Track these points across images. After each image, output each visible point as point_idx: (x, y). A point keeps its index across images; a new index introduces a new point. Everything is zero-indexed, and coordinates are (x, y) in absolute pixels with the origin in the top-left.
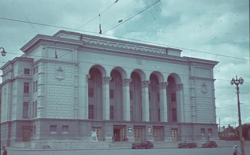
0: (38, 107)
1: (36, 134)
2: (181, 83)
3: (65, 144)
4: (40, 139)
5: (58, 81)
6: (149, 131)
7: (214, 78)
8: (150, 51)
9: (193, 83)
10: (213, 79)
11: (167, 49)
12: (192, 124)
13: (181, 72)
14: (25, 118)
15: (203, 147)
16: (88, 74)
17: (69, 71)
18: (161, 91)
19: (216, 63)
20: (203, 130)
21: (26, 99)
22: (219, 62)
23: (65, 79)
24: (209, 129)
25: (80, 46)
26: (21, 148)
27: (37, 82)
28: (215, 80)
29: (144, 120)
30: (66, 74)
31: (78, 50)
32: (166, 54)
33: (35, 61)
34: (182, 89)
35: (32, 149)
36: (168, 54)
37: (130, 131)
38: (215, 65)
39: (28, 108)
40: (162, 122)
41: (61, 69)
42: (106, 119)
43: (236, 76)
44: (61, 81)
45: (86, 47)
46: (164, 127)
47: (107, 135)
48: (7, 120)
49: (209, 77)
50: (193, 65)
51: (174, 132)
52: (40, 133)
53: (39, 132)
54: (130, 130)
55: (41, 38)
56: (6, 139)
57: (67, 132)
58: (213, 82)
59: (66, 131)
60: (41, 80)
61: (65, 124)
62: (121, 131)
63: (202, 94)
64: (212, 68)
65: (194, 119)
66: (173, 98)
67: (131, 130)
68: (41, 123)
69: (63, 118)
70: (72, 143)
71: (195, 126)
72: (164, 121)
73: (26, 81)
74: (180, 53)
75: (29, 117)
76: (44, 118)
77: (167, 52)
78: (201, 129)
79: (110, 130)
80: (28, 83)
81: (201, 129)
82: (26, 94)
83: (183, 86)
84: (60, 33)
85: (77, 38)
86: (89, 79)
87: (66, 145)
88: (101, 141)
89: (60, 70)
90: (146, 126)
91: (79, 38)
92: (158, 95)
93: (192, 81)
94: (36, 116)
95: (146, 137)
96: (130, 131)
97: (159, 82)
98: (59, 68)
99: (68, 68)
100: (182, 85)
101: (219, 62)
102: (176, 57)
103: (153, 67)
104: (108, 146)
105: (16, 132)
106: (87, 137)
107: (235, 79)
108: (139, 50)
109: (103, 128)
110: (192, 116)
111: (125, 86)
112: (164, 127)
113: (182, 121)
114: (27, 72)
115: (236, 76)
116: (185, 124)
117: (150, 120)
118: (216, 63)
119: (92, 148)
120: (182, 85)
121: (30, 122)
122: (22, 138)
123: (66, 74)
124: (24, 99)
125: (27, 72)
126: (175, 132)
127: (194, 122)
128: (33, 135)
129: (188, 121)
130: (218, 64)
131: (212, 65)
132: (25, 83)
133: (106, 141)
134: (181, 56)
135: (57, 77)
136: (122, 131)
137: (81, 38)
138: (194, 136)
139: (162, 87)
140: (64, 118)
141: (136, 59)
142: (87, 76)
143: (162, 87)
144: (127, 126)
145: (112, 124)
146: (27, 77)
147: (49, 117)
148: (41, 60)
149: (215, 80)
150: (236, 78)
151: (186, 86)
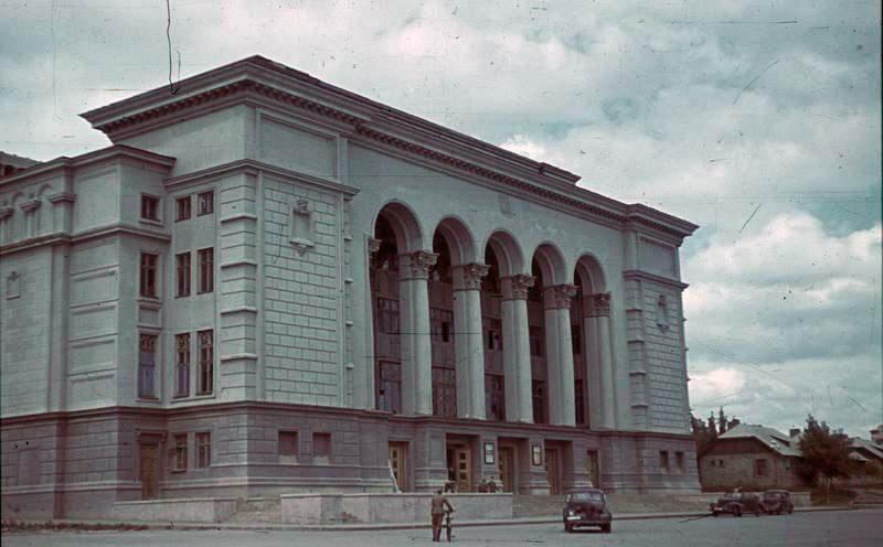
1: (213, 465)
2: (605, 292)
3: (401, 503)
4: (250, 486)
5: (297, 256)
6: (490, 459)
7: (683, 281)
9: (636, 293)
10: (679, 282)
12: (638, 437)
14: (146, 397)
15: (716, 514)
16: (373, 235)
20: (288, 436)
21: (150, 322)
22: (82, 115)
23: (318, 251)
24: (316, 435)
28: (686, 286)
29: (459, 416)
30: (320, 228)
33: (180, 171)
34: (608, 313)
35: (361, 522)
39: (153, 356)
40: (463, 417)
41: (305, 208)
42: (422, 412)
44: (306, 255)
45: (376, 136)
46: (569, 442)
47: (432, 471)
48: (43, 397)
49: (669, 276)
50: (636, 232)
52: (249, 459)
53: (246, 455)
55: (251, 78)
56: (51, 487)
57: (326, 458)
59: (322, 456)
60: (245, 245)
61: (322, 426)
62: (458, 456)
63: (657, 332)
68: (252, 422)
69: (327, 404)
70: (422, 500)
71: (647, 442)
73: (151, 248)
75: (158, 396)
76: (259, 400)
78: (281, 433)
79: (433, 449)
81: (281, 433)
83: (610, 302)
87: (404, 506)
88: (409, 491)
89: (302, 214)
90: (527, 439)
93: (634, 284)
94: (206, 384)
95: (531, 479)
99: (323, 208)
100: (608, 297)
101: (82, 115)
103: (540, 228)
104: (511, 513)
105: (119, 456)
106: (379, 477)
109: (411, 444)
110: (634, 407)
111: (466, 290)
112: (569, 442)
113: (610, 425)
114: (148, 212)
116: (621, 434)
117: (377, 407)
119: (472, 517)
121: (165, 416)
122: (139, 484)
123: (320, 228)
124: (140, 320)
125: (148, 212)
126: (398, 454)
127: (642, 428)
128: (190, 469)
130: (694, 233)
132: (144, 256)
135: (295, 240)
136: (463, 456)
138: (645, 478)
139: (559, 302)
140: (330, 402)
141: (497, 194)
142: (370, 242)
143: (559, 302)
144: (530, 441)
145: (442, 431)
146: (148, 228)
151: (618, 304)
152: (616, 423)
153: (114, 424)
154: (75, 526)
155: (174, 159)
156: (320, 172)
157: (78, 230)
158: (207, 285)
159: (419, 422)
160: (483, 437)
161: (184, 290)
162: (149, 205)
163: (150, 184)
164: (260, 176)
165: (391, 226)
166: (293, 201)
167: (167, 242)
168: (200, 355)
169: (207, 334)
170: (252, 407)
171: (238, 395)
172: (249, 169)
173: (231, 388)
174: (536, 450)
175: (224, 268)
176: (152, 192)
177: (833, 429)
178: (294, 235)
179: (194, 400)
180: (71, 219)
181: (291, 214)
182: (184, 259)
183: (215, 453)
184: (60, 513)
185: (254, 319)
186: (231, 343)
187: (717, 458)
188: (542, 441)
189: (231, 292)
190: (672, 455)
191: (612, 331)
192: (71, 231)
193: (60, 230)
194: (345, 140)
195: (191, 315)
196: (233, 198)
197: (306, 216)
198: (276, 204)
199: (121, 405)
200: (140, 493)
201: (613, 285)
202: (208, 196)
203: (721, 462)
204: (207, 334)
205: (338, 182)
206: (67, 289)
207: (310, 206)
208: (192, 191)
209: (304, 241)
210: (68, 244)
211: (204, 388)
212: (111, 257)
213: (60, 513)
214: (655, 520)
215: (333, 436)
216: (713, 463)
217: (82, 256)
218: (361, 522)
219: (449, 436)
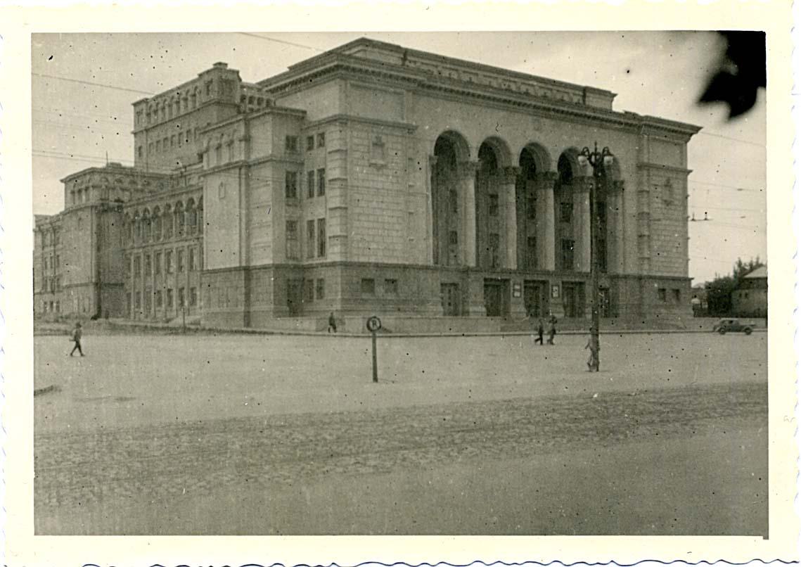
0: (328, 234)
2: (621, 179)
6: (555, 295)
7: (689, 168)
8: (455, 76)
11: (585, 91)
13: (622, 151)
17: (394, 143)
18: (577, 197)
19: (696, 129)
25: (421, 85)
26: (567, 334)
27: (322, 171)
28: (691, 171)
31: (414, 93)
32: (581, 102)
36: (587, 103)
37: (517, 294)
38: (691, 135)
41: (380, 141)
43: (596, 144)
49: (678, 166)
51: (450, 291)
54: (517, 290)
58: (687, 176)
64: (686, 142)
65: (646, 267)
66: (600, 211)
67: (520, 291)
72: (509, 267)
74: (612, 101)
77: (584, 96)
78: (363, 280)
79: (475, 289)
80: (294, 174)
82: (291, 201)
83: (624, 186)
84: (361, 44)
85: (394, 60)
86: (433, 166)
89: (378, 144)
91: (399, 57)
92: (454, 193)
94: (322, 251)
96: (517, 294)
97: (538, 170)
98: (376, 138)
100: (622, 182)
102: (601, 110)
107: (592, 150)
108: (470, 82)
113: (620, 272)
115: (596, 144)
118: (696, 129)
120: (622, 182)
127: (645, 273)
128: (315, 300)
129: (632, 270)
131: (684, 133)
132: (288, 173)
133: (472, 316)
134: (614, 109)
135: (373, 161)
137: (404, 59)
142: (431, 158)
147: (369, 259)
148: (331, 121)
149: (691, 171)
150: (594, 147)
151: (630, 188)
152: (624, 270)
153: (338, 271)
154: (260, 333)
155: (305, 112)
156: (390, 117)
157: (253, 157)
158: (322, 193)
159: (467, 271)
160: (551, 282)
161: (311, 195)
162: (291, 143)
163: (290, 129)
164: (349, 123)
165: (447, 147)
166: (373, 136)
167: (302, 164)
168: (318, 230)
169: (322, 221)
170: (346, 265)
171: (338, 259)
172: (341, 120)
173: (334, 253)
174: (555, 288)
175: (330, 181)
176: (292, 133)
177: (711, 280)
178: (373, 158)
179: (317, 261)
180: (248, 151)
181: (371, 145)
182: (311, 174)
183: (326, 291)
184: (248, 325)
185: (346, 212)
186: (333, 228)
187: (744, 292)
188: (560, 282)
189: (334, 196)
190: (668, 291)
191: (627, 206)
192: (249, 158)
193: (243, 158)
194: (411, 94)
195: (316, 210)
196: (334, 138)
197: (382, 145)
198: (359, 138)
199: (277, 262)
200: (288, 314)
201: (626, 173)
202: (322, 136)
203: (746, 295)
204: (322, 221)
205: (405, 122)
206: (248, 196)
207: (384, 139)
208: (314, 133)
209: (381, 162)
210: (248, 166)
211: (322, 253)
212: (267, 172)
213: (248, 325)
214: (426, 338)
215: (376, 281)
216: (740, 295)
217: (255, 172)
218: (391, 332)
219: (485, 280)
